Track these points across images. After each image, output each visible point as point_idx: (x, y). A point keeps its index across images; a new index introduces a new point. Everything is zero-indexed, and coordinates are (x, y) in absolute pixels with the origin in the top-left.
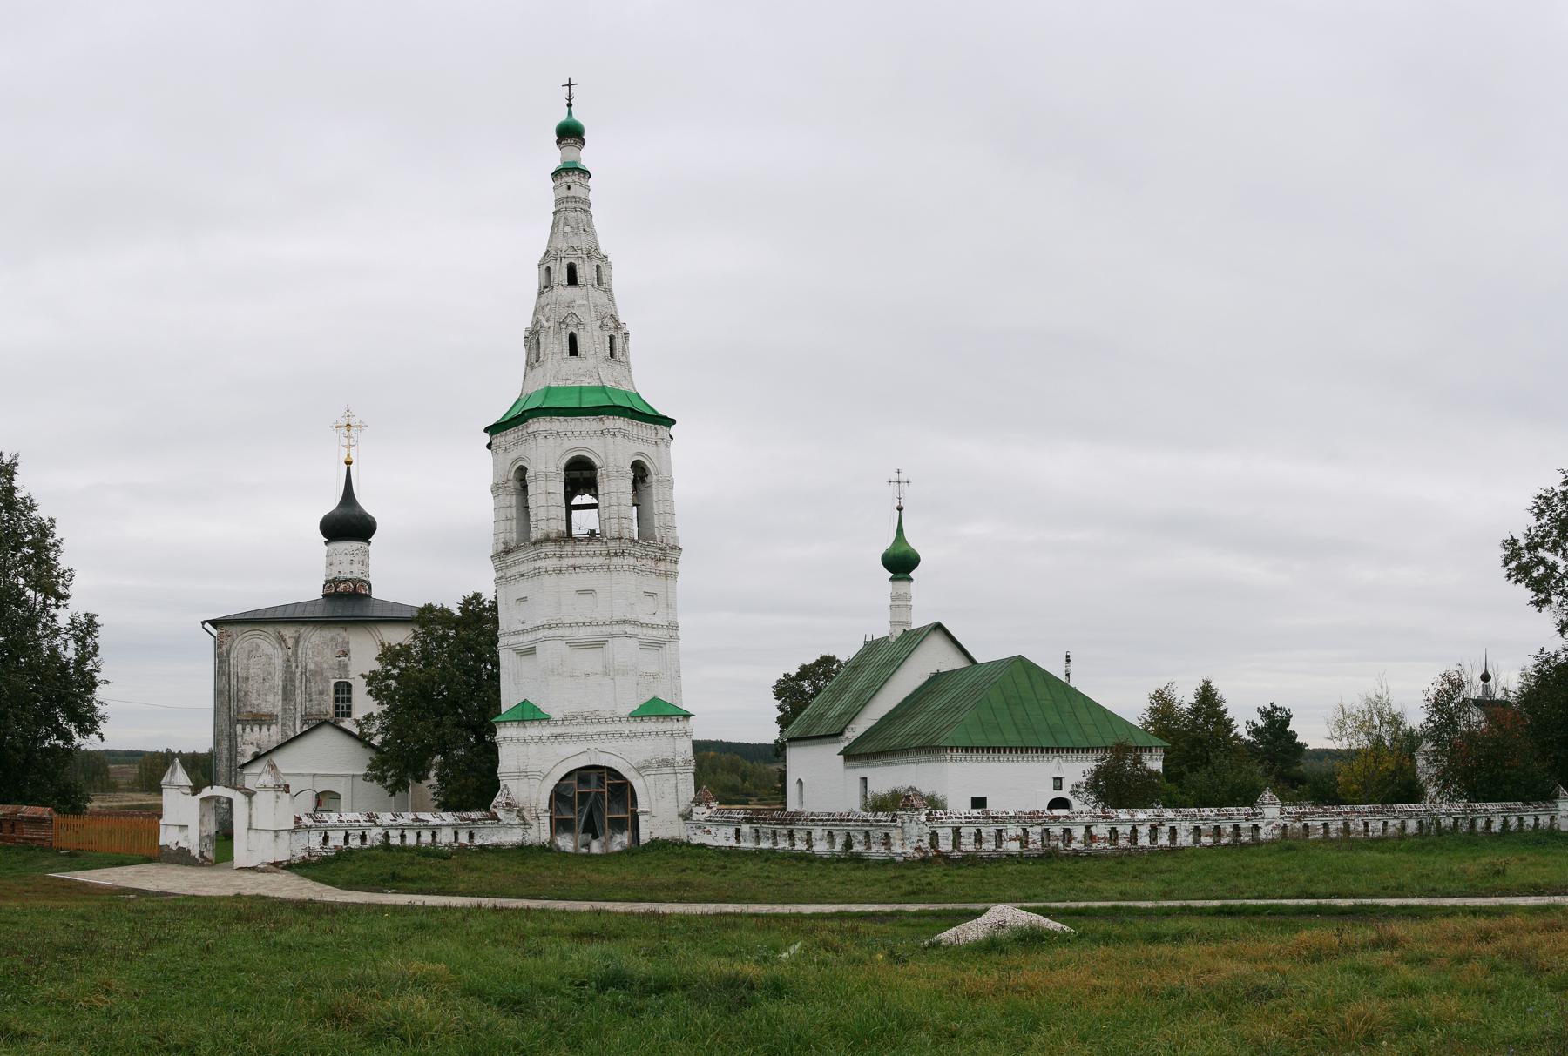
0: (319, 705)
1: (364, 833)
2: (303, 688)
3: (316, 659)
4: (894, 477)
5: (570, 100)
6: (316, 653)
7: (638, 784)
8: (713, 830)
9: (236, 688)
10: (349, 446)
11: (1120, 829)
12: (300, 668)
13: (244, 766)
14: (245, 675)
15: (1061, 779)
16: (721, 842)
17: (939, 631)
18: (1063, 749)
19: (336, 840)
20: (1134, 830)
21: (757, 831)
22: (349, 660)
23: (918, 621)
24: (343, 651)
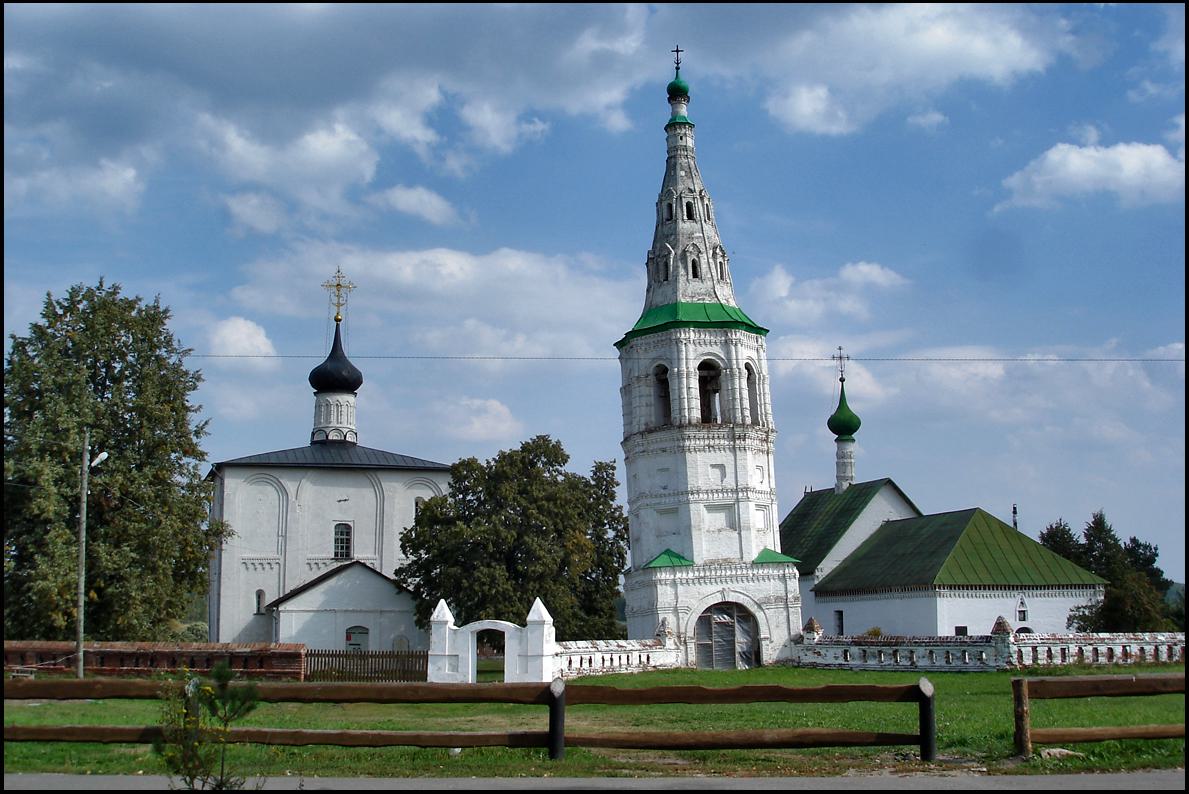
4: (837, 353)
5: (678, 64)
7: (760, 615)
8: (823, 652)
10: (339, 305)
11: (1147, 648)
15: (1024, 612)
16: (830, 660)
17: (889, 487)
18: (972, 586)
20: (1157, 649)
21: (864, 651)
23: (859, 475)
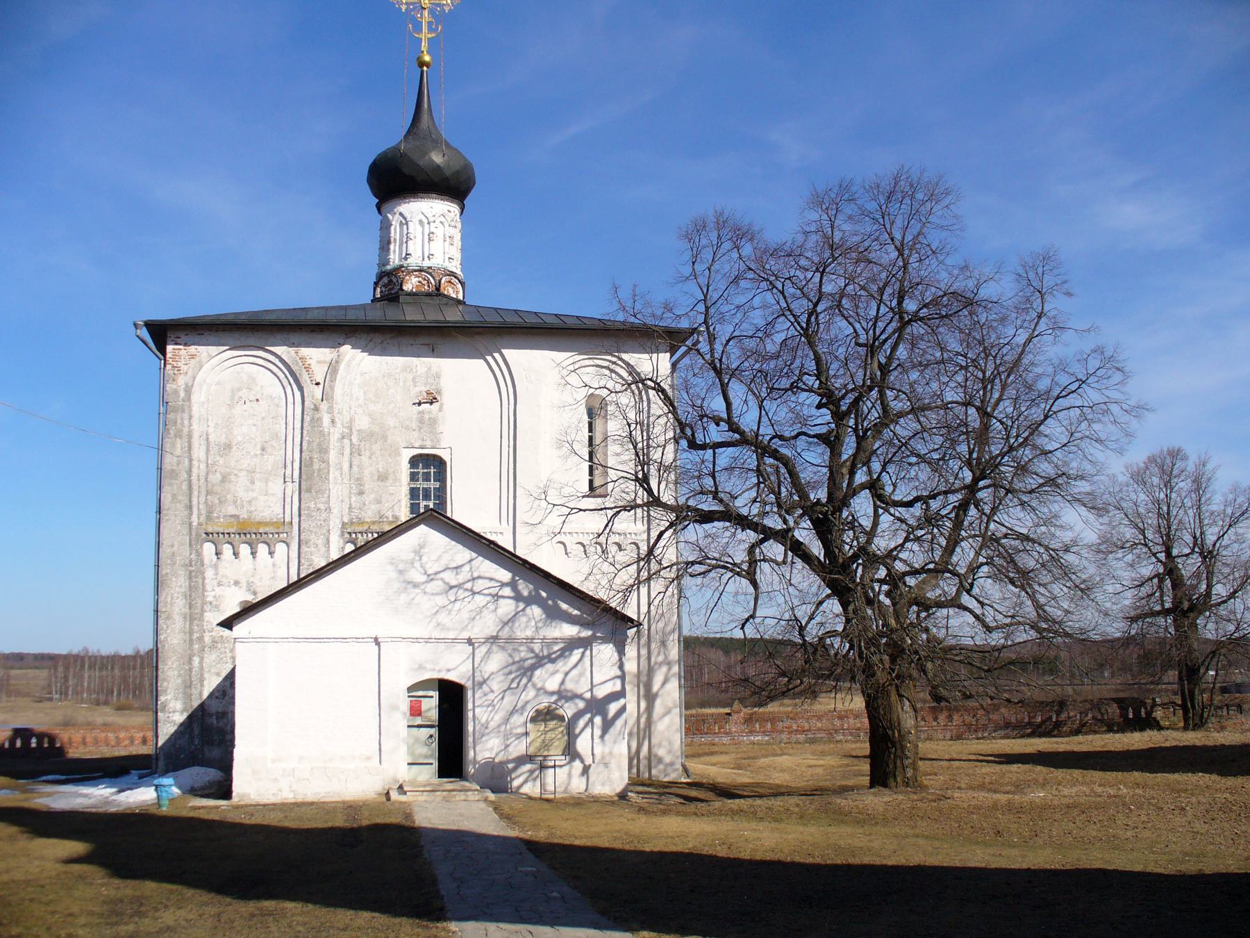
0: (379, 502)
2: (346, 466)
9: (203, 466)
12: (339, 425)
14: (223, 440)
22: (440, 410)
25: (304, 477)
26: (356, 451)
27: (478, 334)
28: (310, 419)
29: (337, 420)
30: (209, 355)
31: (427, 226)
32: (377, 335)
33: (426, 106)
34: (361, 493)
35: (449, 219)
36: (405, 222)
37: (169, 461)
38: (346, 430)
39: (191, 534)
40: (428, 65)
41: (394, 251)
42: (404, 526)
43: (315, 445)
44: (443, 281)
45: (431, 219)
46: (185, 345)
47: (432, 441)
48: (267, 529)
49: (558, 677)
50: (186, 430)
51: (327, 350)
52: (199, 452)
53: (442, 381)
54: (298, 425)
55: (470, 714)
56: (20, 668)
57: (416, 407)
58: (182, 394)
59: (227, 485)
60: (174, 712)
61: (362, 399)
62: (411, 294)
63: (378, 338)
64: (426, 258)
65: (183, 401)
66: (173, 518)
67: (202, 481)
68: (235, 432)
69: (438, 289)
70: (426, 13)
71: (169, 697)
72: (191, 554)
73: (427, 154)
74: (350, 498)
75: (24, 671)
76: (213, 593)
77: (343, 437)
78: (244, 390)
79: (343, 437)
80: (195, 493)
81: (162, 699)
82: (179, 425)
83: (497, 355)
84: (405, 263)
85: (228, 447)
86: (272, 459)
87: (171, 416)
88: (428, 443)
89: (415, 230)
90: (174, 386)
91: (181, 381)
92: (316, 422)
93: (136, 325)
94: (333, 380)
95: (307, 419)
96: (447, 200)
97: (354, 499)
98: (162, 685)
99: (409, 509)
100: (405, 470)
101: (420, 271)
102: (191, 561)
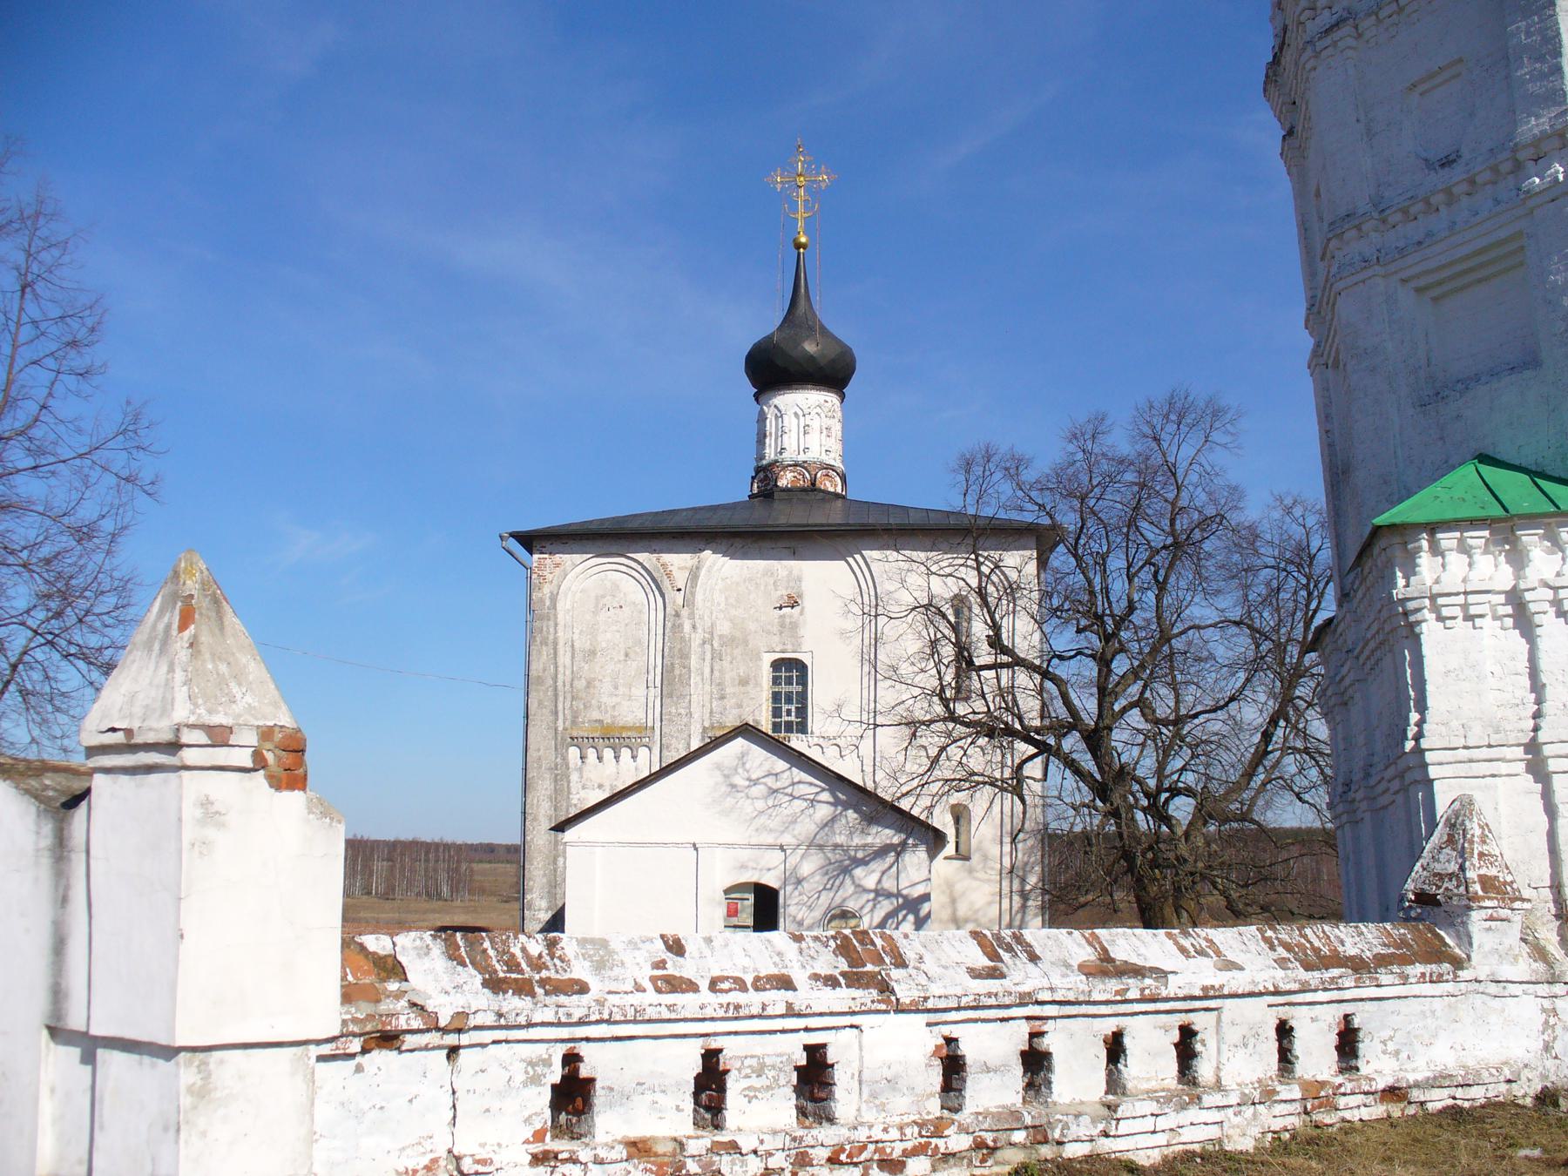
0: (740, 706)
1: (816, 1053)
2: (707, 671)
3: (733, 612)
6: (732, 600)
9: (568, 672)
12: (700, 630)
13: (1276, 1101)
14: (587, 646)
19: (641, 1102)
22: (802, 613)
24: (790, 597)
25: (665, 682)
26: (717, 656)
27: (839, 536)
28: (672, 625)
29: (698, 625)
30: (573, 563)
31: (802, 418)
32: (738, 540)
33: (803, 290)
34: (722, 698)
35: (826, 410)
36: (780, 416)
37: (536, 667)
38: (707, 636)
39: (556, 739)
40: (804, 246)
41: (770, 445)
42: (721, 740)
43: (676, 650)
44: (819, 475)
45: (806, 411)
46: (550, 553)
47: (793, 645)
48: (629, 734)
49: (875, 877)
50: (551, 637)
51: (687, 556)
52: (564, 658)
53: (803, 584)
54: (660, 631)
55: (781, 910)
56: (490, 862)
57: (777, 611)
58: (548, 603)
59: (592, 690)
60: (539, 910)
61: (723, 605)
62: (786, 490)
63: (738, 543)
64: (802, 452)
65: (549, 609)
66: (539, 723)
67: (568, 687)
68: (599, 639)
69: (813, 484)
70: (802, 191)
71: (534, 896)
72: (556, 758)
73: (799, 344)
74: (711, 703)
75: (493, 865)
76: (578, 796)
77: (704, 643)
78: (608, 597)
79: (704, 643)
80: (561, 699)
81: (528, 897)
82: (545, 633)
83: (858, 557)
84: (780, 458)
85: (593, 653)
86: (634, 664)
87: (537, 624)
88: (789, 647)
89: (790, 423)
90: (540, 595)
91: (547, 589)
92: (677, 628)
93: (501, 537)
94: (694, 585)
95: (669, 625)
96: (824, 390)
97: (715, 703)
98: (529, 884)
99: (770, 713)
100: (766, 673)
101: (796, 465)
102: (556, 765)
